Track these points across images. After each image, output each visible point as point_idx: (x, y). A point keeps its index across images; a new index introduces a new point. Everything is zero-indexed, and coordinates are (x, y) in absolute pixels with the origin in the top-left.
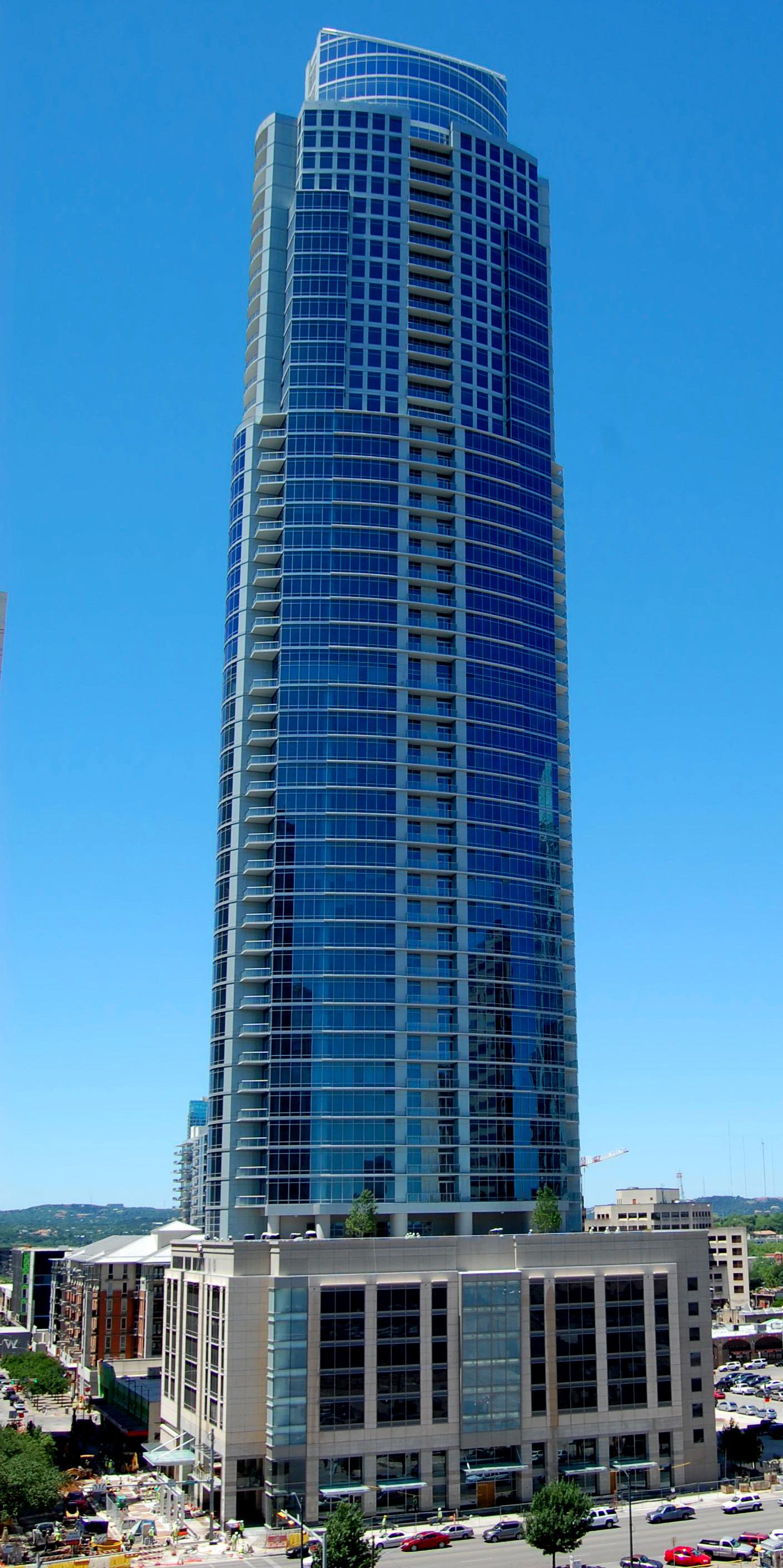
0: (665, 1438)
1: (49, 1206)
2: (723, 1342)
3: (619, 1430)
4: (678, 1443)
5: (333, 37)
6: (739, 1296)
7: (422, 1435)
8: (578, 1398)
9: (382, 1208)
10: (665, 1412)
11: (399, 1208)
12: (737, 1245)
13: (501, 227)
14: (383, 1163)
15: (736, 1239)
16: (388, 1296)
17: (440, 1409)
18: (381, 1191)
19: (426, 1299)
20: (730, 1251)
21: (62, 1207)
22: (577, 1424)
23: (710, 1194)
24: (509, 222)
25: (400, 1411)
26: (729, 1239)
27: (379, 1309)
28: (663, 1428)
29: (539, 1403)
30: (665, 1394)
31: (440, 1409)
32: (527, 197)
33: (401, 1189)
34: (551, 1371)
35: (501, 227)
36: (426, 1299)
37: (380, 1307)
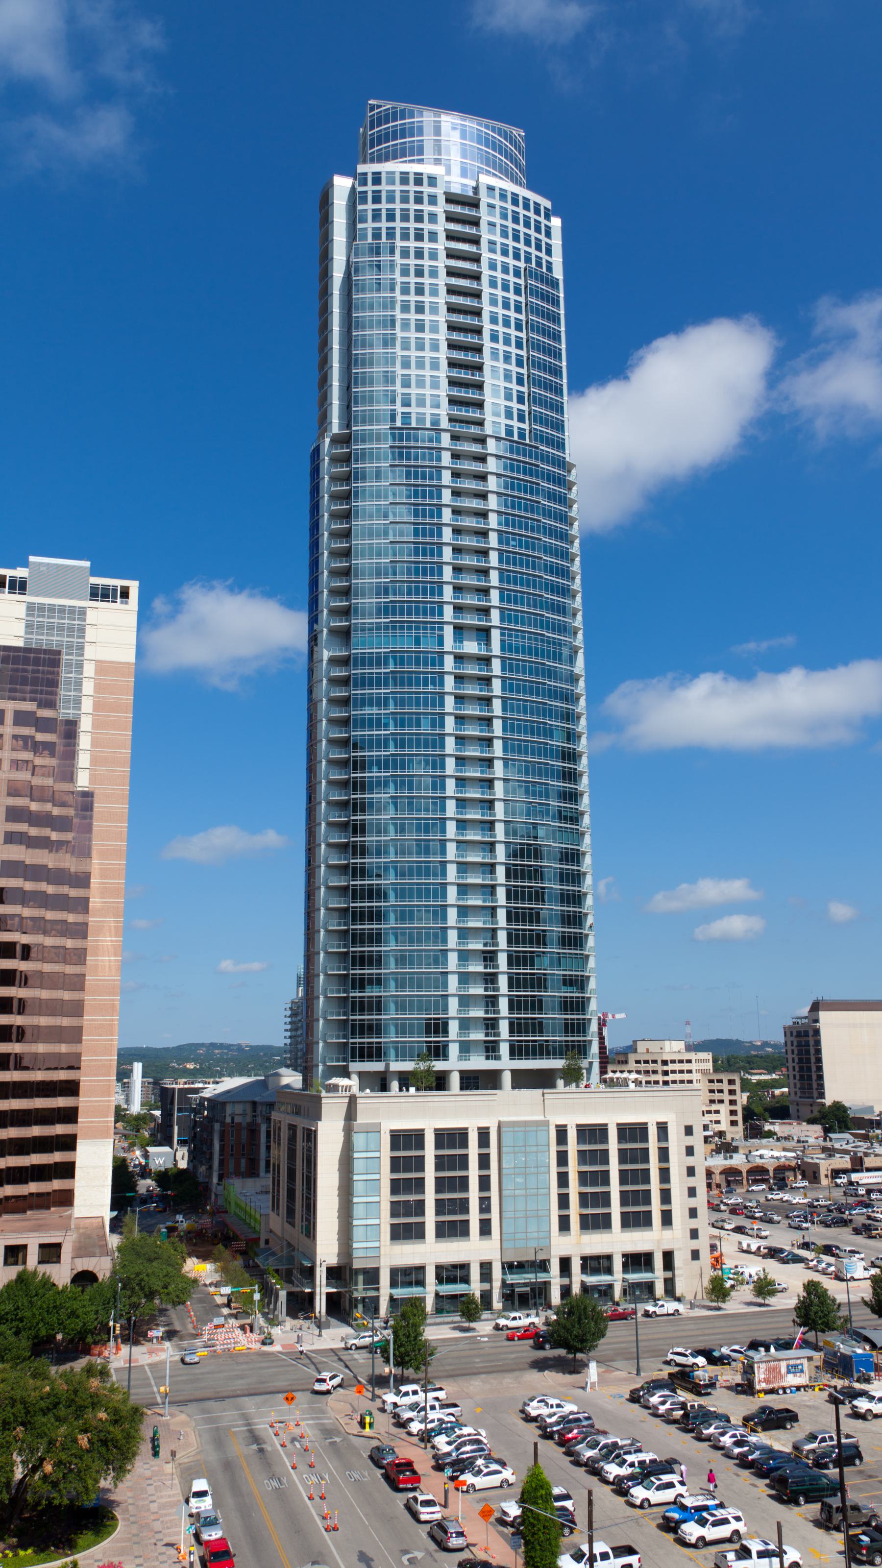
0: (668, 1257)
1: (193, 1045)
2: (721, 1169)
3: (631, 1248)
4: (681, 1260)
5: (379, 107)
6: (734, 1128)
7: (471, 1250)
8: (596, 1223)
9: (439, 1066)
10: (667, 1233)
11: (453, 1064)
12: (732, 1087)
13: (522, 264)
14: (439, 1027)
15: (731, 1082)
16: (445, 1138)
17: (485, 1229)
18: (439, 1051)
19: (473, 1139)
20: (726, 1092)
21: (203, 1045)
22: (596, 1243)
23: (714, 1037)
24: (528, 260)
25: (454, 1230)
26: (725, 1082)
27: (424, 1201)
28: (667, 1247)
29: (564, 1224)
30: (667, 1219)
31: (485, 1229)
32: (542, 237)
33: (454, 1050)
34: (574, 1200)
35: (522, 264)
36: (473, 1139)
37: (422, 1202)
